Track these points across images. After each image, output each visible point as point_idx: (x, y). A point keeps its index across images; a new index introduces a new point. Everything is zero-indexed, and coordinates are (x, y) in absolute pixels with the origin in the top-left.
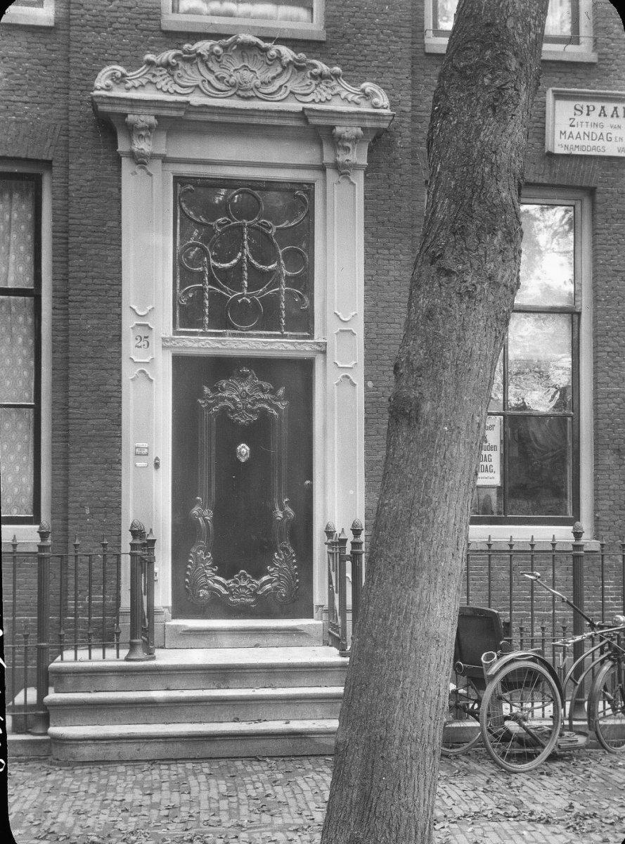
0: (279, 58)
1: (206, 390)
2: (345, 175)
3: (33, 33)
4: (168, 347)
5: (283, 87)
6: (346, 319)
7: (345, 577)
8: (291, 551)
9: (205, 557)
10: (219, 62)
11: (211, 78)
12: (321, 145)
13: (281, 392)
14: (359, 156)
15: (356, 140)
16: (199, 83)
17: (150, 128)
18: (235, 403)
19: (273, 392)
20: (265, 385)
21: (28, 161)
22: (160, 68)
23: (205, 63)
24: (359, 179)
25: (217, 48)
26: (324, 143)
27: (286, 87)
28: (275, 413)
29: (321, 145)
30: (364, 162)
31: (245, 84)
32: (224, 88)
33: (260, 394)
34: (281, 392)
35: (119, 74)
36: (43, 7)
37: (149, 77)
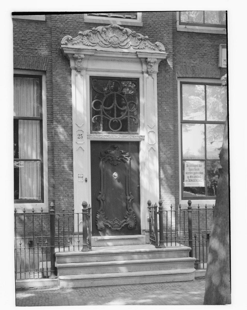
0: (126, 32)
23: (100, 34)
24: (155, 76)
27: (129, 43)
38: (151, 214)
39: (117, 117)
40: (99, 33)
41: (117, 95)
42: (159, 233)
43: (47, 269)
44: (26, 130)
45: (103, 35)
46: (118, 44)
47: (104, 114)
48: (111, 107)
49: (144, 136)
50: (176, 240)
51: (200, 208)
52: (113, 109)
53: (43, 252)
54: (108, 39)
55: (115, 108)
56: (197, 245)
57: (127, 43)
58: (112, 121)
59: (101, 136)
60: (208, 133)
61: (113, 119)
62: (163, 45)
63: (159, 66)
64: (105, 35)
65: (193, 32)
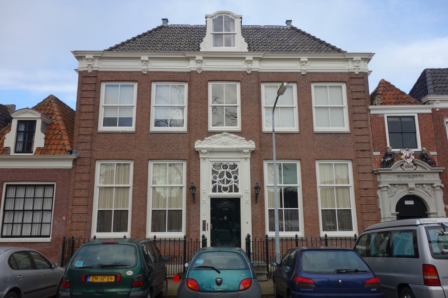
0: (232, 136)
1: (218, 204)
2: (246, 160)
3: (71, 159)
4: (209, 197)
8: (236, 238)
13: (233, 204)
14: (249, 156)
17: (206, 153)
18: (224, 206)
19: (232, 203)
20: (230, 202)
25: (219, 136)
28: (232, 208)
30: (250, 157)
32: (221, 143)
33: (229, 204)
34: (233, 204)
35: (200, 142)
36: (352, 231)
37: (206, 142)
38: (397, 231)
41: (227, 172)
43: (179, 264)
45: (219, 139)
47: (218, 183)
48: (223, 178)
49: (242, 195)
50: (290, 227)
51: (303, 239)
52: (224, 180)
54: (221, 140)
58: (223, 187)
62: (253, 142)
63: (251, 154)
65: (265, 26)
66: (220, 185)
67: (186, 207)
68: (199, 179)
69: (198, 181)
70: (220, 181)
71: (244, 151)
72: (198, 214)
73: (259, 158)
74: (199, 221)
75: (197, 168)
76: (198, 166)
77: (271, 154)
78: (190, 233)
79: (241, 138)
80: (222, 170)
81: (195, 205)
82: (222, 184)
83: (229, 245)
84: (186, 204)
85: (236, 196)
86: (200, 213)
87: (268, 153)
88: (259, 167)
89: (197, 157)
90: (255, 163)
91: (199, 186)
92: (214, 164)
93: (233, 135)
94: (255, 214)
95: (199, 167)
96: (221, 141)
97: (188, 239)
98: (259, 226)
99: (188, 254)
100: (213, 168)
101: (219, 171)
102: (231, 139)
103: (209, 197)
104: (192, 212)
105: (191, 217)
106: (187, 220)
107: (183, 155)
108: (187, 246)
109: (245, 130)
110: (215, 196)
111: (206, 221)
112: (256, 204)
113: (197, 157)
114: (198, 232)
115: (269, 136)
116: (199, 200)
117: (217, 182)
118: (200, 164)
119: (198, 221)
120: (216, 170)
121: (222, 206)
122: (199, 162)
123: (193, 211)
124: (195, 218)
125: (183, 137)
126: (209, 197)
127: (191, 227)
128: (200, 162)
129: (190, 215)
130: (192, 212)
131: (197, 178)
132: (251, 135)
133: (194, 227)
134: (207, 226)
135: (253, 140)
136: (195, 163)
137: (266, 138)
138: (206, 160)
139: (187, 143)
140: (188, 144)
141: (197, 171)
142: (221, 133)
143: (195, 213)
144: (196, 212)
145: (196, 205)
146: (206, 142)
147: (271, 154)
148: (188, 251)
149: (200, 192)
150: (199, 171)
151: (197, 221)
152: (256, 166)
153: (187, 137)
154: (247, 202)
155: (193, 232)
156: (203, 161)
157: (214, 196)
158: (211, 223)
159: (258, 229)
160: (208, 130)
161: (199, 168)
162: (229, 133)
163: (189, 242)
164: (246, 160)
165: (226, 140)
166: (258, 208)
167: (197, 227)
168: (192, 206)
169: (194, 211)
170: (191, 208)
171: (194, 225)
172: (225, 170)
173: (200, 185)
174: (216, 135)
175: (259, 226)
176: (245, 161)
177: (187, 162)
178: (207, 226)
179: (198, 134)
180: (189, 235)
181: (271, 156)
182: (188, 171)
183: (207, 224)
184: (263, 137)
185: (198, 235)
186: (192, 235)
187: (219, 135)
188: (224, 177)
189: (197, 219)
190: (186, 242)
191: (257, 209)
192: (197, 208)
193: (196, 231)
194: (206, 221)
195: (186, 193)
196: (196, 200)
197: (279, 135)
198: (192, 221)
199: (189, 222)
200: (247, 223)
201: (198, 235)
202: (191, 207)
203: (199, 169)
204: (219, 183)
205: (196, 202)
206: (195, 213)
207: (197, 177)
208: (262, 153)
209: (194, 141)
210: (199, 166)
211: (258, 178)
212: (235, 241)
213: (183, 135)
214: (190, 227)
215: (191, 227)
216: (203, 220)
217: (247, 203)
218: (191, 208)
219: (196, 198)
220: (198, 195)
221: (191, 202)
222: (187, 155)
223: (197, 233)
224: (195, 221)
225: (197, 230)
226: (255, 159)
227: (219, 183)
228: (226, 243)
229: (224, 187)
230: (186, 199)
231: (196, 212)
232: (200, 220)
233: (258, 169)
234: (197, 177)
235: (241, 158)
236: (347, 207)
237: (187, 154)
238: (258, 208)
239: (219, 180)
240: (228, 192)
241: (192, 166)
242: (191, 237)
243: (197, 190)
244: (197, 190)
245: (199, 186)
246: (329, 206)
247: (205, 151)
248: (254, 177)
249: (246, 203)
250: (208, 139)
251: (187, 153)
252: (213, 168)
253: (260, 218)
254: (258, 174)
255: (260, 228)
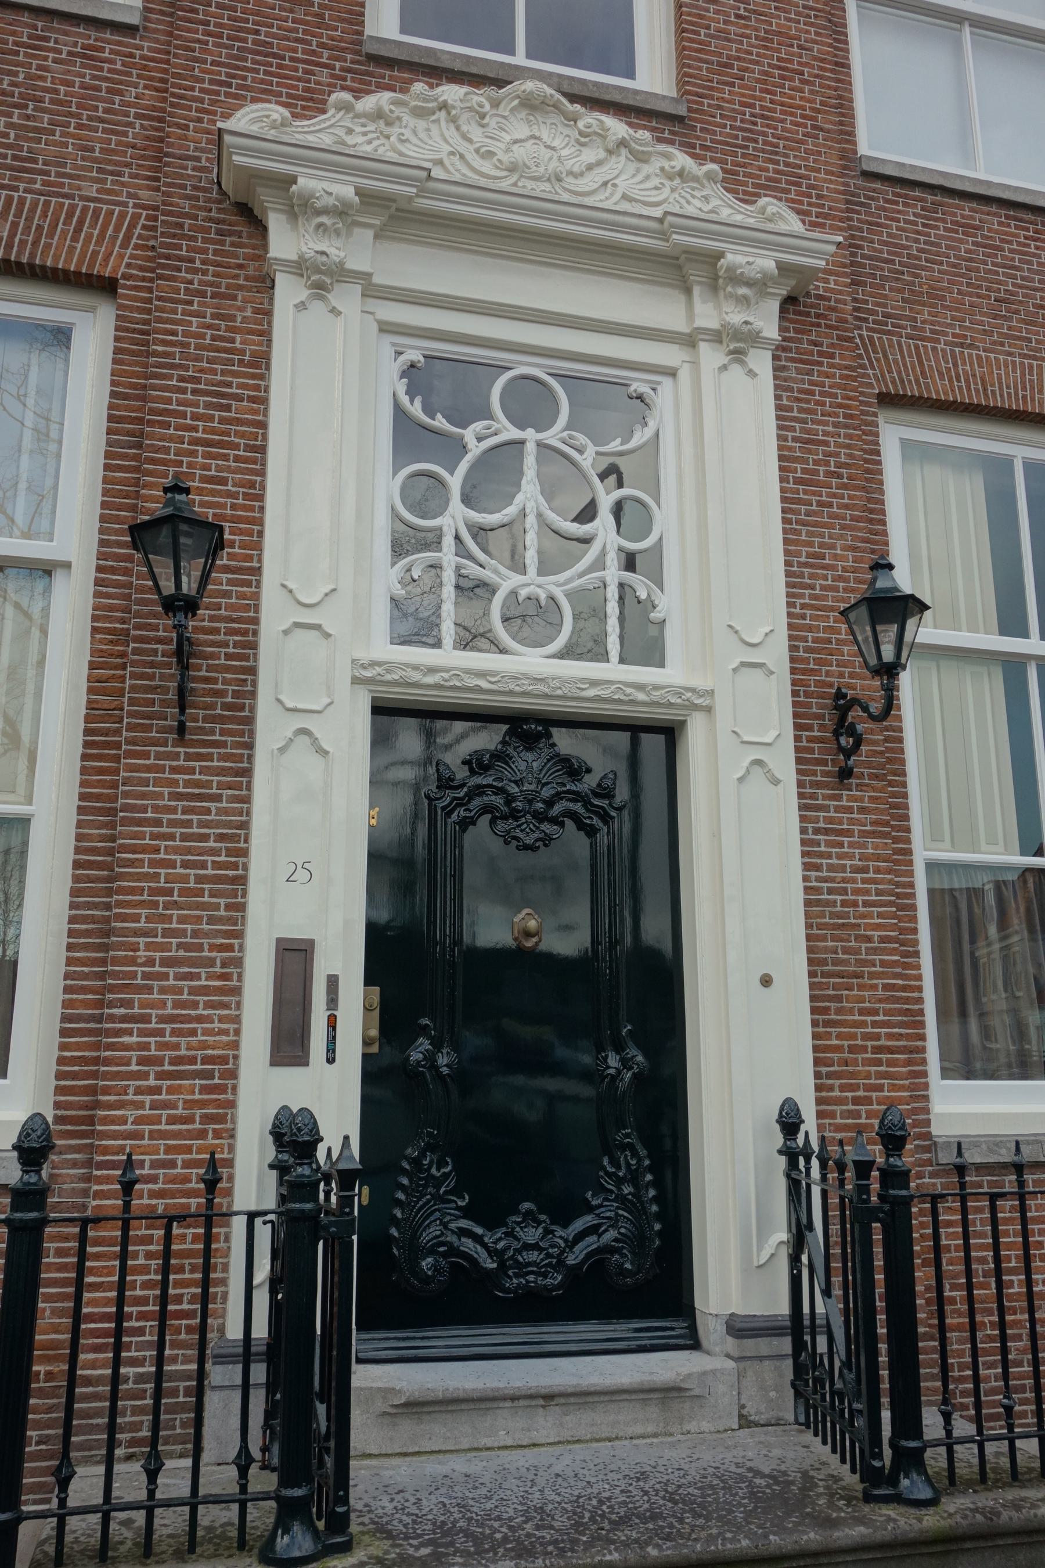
0: (602, 135)
2: (738, 355)
5: (609, 185)
6: (755, 640)
7: (872, 1280)
8: (643, 1152)
9: (438, 1170)
10: (483, 126)
11: (463, 147)
12: (688, 291)
15: (760, 285)
16: (444, 156)
17: (341, 211)
18: (509, 799)
21: (35, 742)
22: (363, 120)
23: (453, 120)
24: (762, 362)
26: (696, 291)
27: (615, 185)
29: (688, 291)
31: (535, 168)
33: (565, 779)
39: (541, 573)
40: (449, 113)
42: (263, 1366)
44: (20, 832)
45: (476, 133)
46: (553, 179)
49: (711, 693)
53: (985, 960)
55: (531, 521)
56: (935, 1391)
57: (605, 184)
58: (514, 593)
59: (445, 675)
60: (210, 1450)
61: (516, 579)
64: (481, 130)
66: (472, 569)
67: (83, 784)
68: (252, 485)
69: (234, 507)
70: (479, 532)
71: (735, 257)
72: (217, 865)
73: (846, 368)
74: (230, 948)
75: (235, 374)
76: (243, 352)
77: (937, 360)
78: (106, 1091)
79: (682, 160)
80: (496, 425)
81: (189, 757)
82: (502, 569)
83: (565, 1226)
84: (87, 744)
85: (641, 696)
86: (245, 853)
87: (917, 347)
88: (848, 446)
89: (240, 267)
90: (817, 403)
91: (249, 558)
92: (416, 356)
93: (617, 127)
94: (830, 891)
95: (262, 361)
96: (501, 155)
97: (75, 1164)
98: (875, 1024)
99: (73, 1360)
100: (405, 400)
101: (469, 435)
102: (590, 155)
103: (356, 681)
104: (154, 836)
105: (132, 891)
106: (87, 933)
107: (78, 230)
108: (60, 1253)
109: (720, 107)
110: (430, 680)
111: (311, 942)
112: (838, 798)
113: (240, 267)
114: (209, 1075)
115: (915, 206)
116: (242, 708)
117: (448, 541)
118: (266, 334)
119: (221, 948)
120: (440, 422)
121: (499, 801)
122: (257, 311)
123: (158, 823)
124: (176, 905)
125: (89, 56)
126: (356, 681)
127: (124, 1019)
128: (269, 313)
129: (121, 877)
130: (154, 836)
131: (228, 469)
132: (772, 161)
133: (162, 1019)
134: (332, 1001)
135: (793, 201)
136: (214, 316)
137: (892, 219)
138: (333, 299)
139: (131, 125)
140: (147, 138)
141: (239, 398)
142: (500, 83)
143: (189, 851)
144: (204, 838)
145: (200, 757)
146: (341, 132)
147: (937, 360)
148: (77, 1317)
149: (256, 621)
150: (252, 400)
151: (212, 947)
152: (826, 433)
153: (134, 65)
154: (758, 762)
155: (152, 1082)
156: (301, 306)
157: (415, 676)
158: (369, 980)
159: (864, 1049)
160: (361, 33)
161: (253, 376)
162: (573, 98)
163: (85, 1223)
164: (738, 355)
165: (545, 153)
166: (863, 834)
167: (200, 1019)
168: (148, 769)
169: (172, 823)
170: (143, 796)
171: (162, 990)
172: (530, 435)
173: (258, 546)
174: (451, 92)
175: (875, 1024)
176: (724, 368)
177: (119, 317)
178: (332, 1001)
179: (263, 49)
180: (91, 1120)
181: (941, 374)
182: (125, 397)
183: (333, 982)
184: (862, 204)
185: (207, 1119)
186: (131, 1114)
187: (480, 97)
188: (519, 498)
189: (211, 920)
190: (45, 1222)
191: (851, 845)
192: (218, 798)
193: (192, 1060)
194: (311, 942)
195: (95, 630)
196: (212, 706)
197: (994, 214)
198: (148, 946)
199: (103, 962)
200: (766, 981)
201: (207, 1119)
202: (146, 782)
203: (257, 388)
204: (471, 558)
205: (201, 730)
206: (189, 851)
207: (225, 457)
208: (861, 336)
209: (213, 102)
210: (254, 354)
211: (853, 549)
212: (634, 1177)
213: (83, 37)
214: (112, 1018)
215: (124, 1019)
216: (279, 941)
217: (757, 770)
218: (143, 796)
219: (206, 680)
220: (229, 657)
221: (148, 728)
222: (128, 237)
223: (204, 1089)
224: (187, 947)
225: (206, 1060)
226: (809, 373)
227: (471, 558)
228: (526, 1206)
229: (523, 593)
230: (90, 691)
231: (204, 838)
232: (239, 935)
233: (846, 466)
234: (225, 457)
235: (689, 341)
236: (984, 846)
237: (132, 226)
238: (863, 834)
239: (466, 525)
240: (561, 655)
241: (183, 345)
242: (115, 1135)
243: (226, 594)
244: (226, 594)
245: (249, 558)
246: (992, 841)
247: (336, 189)
248: (810, 534)
249: (748, 771)
250: (365, 115)
251: (122, 216)
252: (405, 400)
253: (882, 940)
254: (846, 507)
255: (890, 1036)
